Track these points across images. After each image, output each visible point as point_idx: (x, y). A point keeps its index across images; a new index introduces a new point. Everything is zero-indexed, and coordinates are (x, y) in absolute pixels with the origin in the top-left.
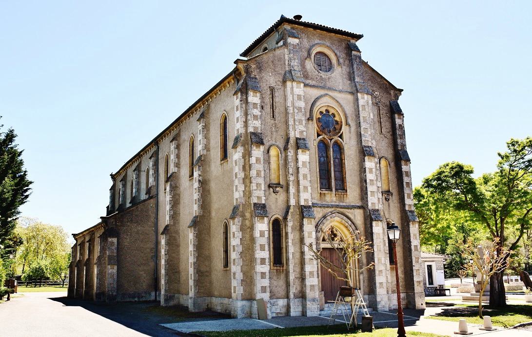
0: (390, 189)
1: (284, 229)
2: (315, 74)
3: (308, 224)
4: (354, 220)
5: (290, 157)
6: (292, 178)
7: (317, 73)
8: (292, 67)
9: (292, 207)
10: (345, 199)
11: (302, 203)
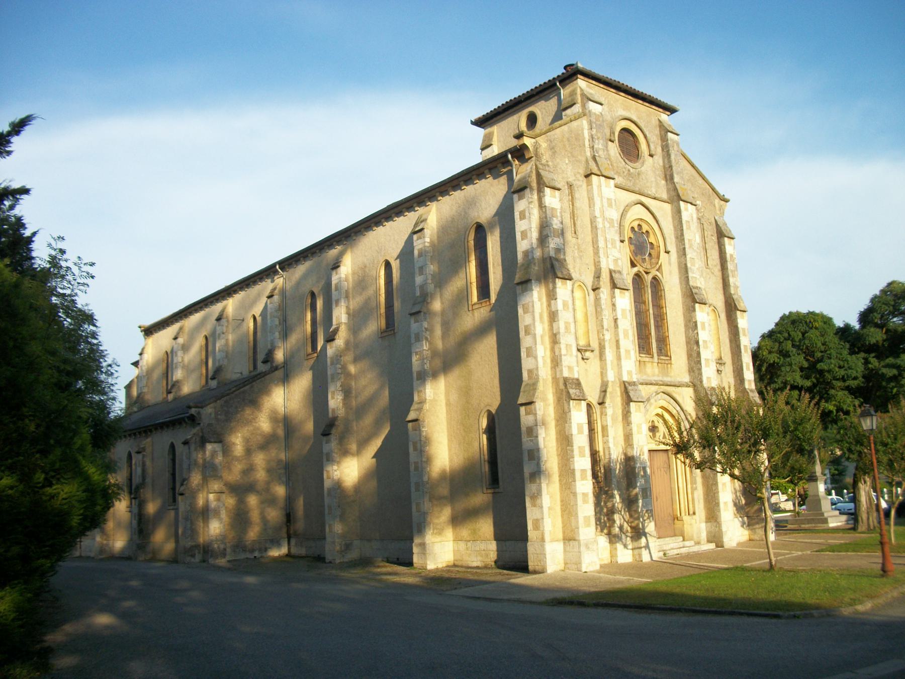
0: (722, 356)
1: (599, 421)
2: (621, 165)
3: (636, 412)
4: (683, 405)
5: (603, 302)
6: (608, 336)
7: (624, 163)
8: (596, 151)
9: (610, 384)
10: (669, 369)
11: (625, 378)
